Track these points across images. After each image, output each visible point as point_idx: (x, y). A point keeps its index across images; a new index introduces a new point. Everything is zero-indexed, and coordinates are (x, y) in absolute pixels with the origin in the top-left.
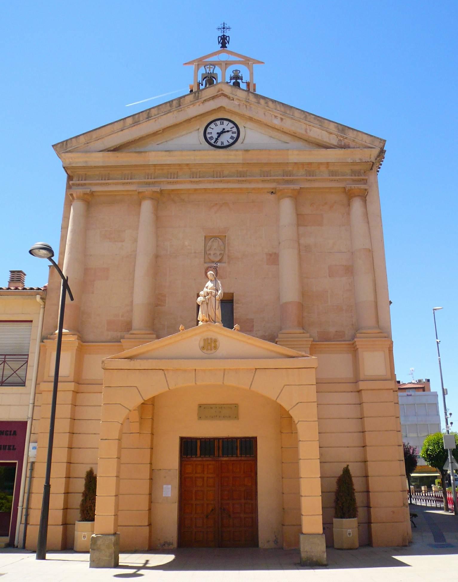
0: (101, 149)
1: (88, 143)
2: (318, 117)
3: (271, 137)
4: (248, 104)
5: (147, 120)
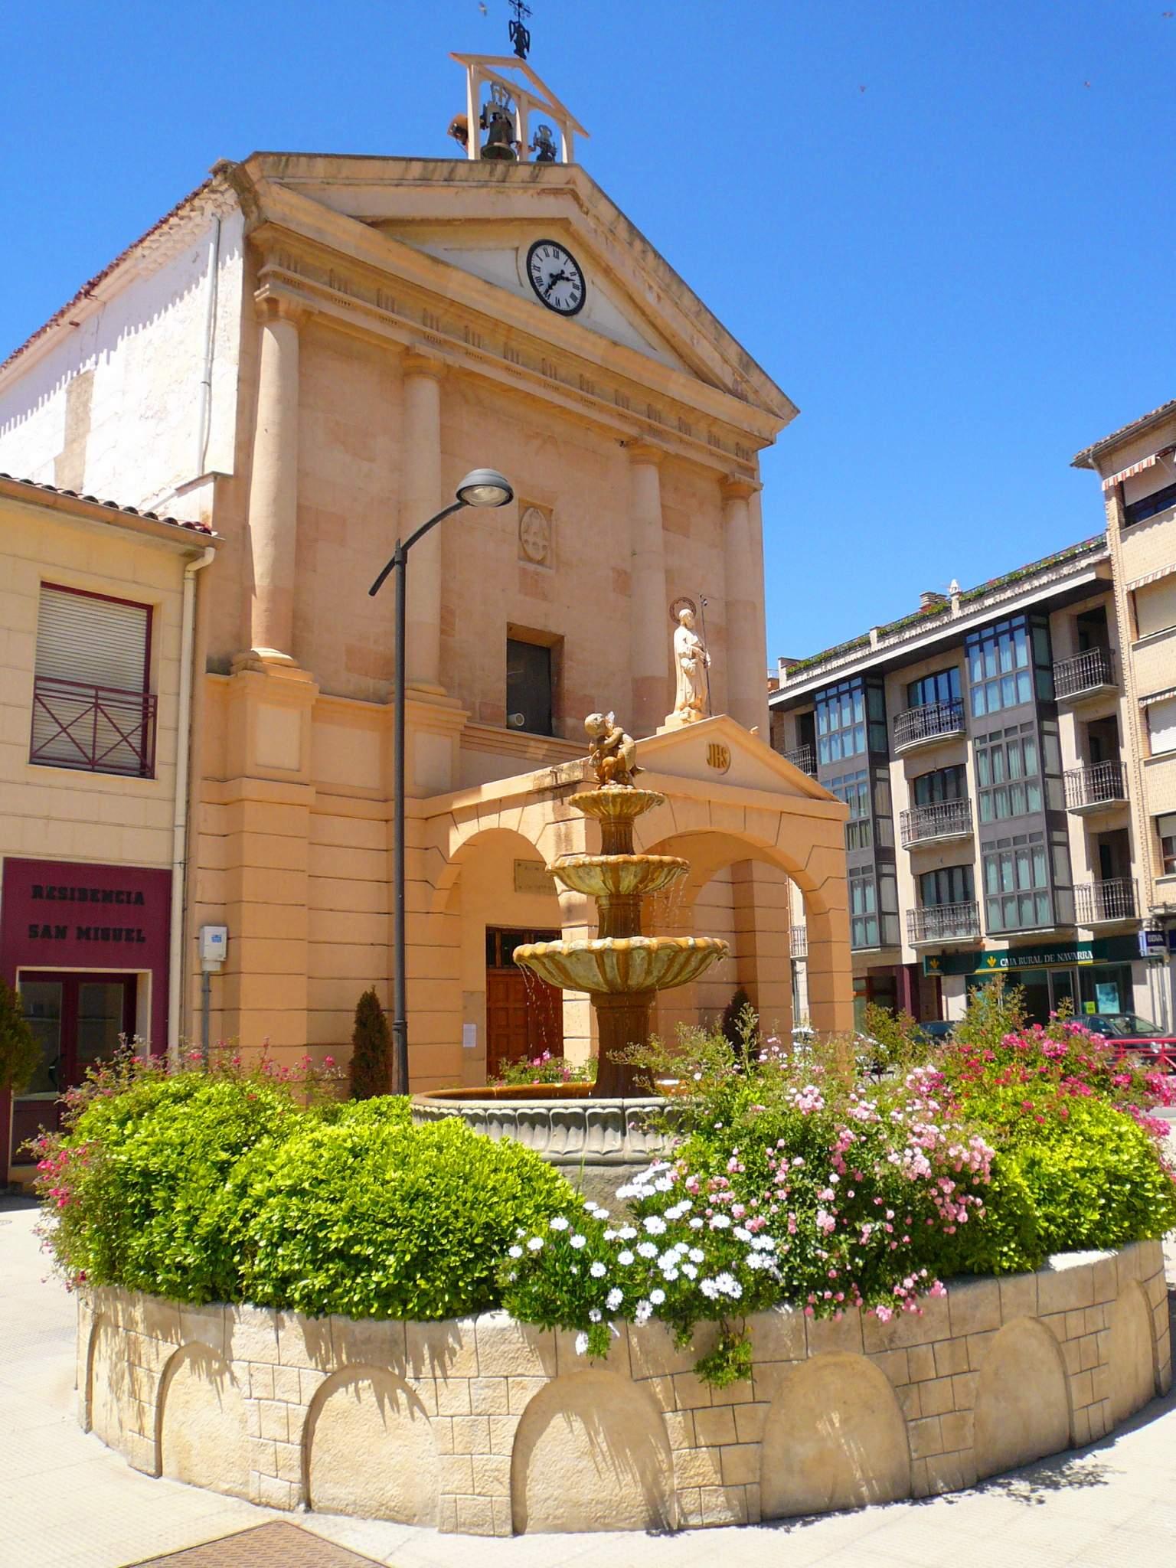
0: (354, 214)
1: (328, 184)
2: (719, 322)
3: (631, 325)
5: (446, 183)
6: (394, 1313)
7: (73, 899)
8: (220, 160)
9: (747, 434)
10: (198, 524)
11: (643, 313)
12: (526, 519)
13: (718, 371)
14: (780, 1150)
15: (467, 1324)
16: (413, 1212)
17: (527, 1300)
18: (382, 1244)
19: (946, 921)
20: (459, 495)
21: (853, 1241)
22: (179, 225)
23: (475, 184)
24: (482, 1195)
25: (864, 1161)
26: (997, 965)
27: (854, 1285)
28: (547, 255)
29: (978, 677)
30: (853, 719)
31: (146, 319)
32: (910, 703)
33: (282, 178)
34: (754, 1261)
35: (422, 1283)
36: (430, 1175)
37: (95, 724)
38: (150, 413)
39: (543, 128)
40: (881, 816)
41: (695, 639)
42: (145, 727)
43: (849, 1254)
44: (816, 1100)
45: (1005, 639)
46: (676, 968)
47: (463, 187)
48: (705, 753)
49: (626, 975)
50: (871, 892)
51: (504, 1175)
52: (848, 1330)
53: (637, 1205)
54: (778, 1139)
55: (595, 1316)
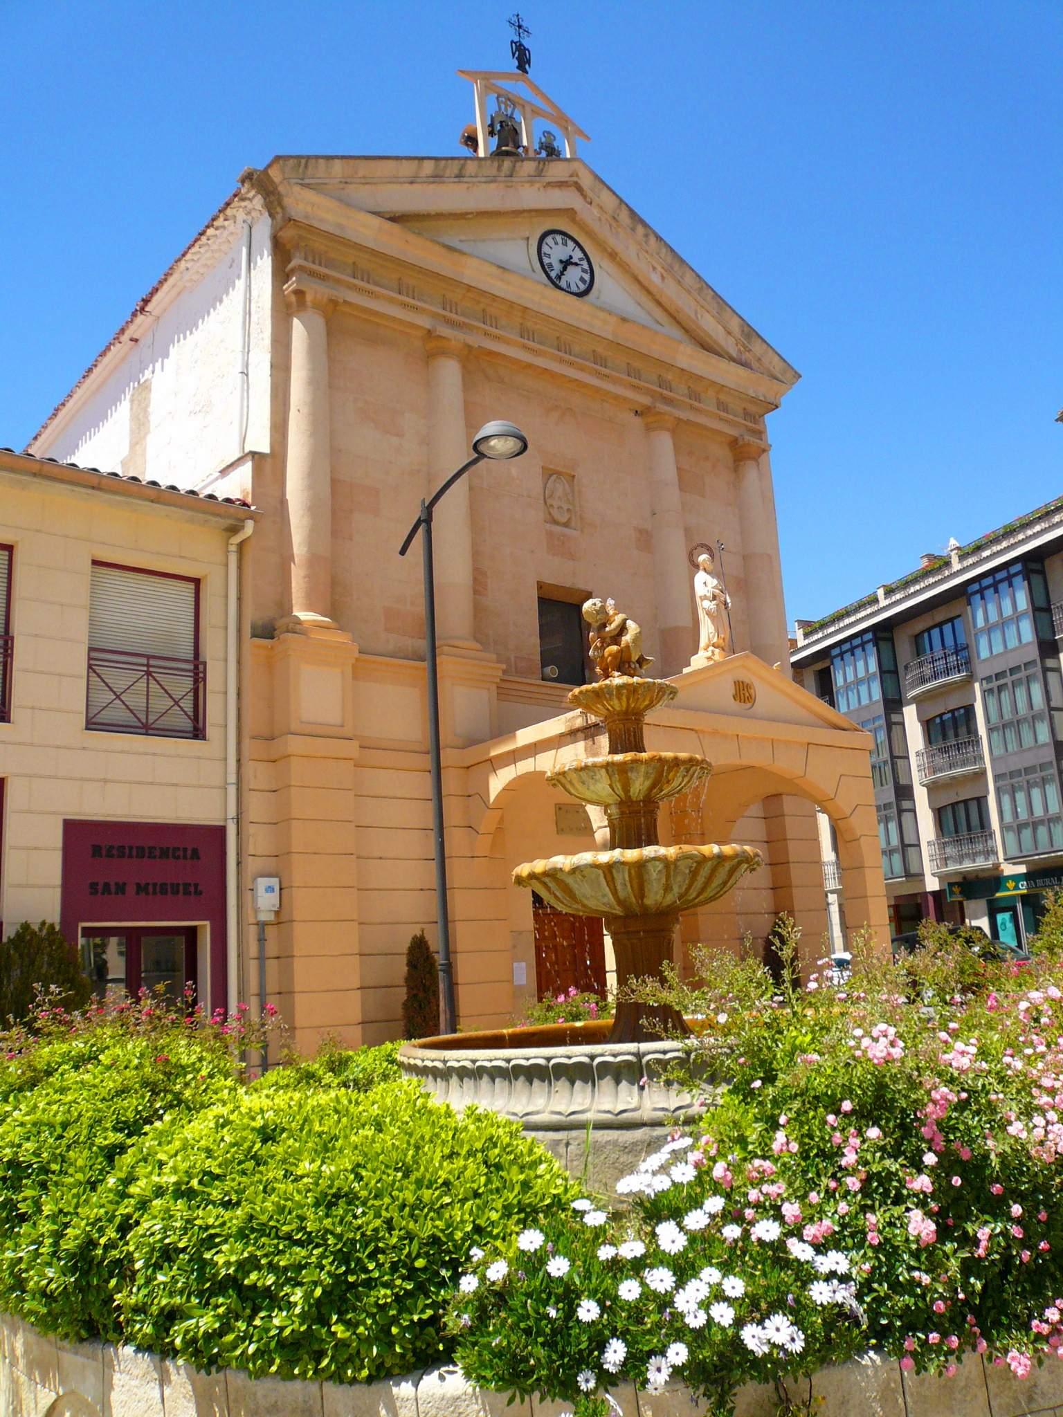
1: (346, 183)
2: (720, 297)
4: (614, 224)
5: (456, 180)
6: (304, 1373)
7: (130, 856)
8: (245, 168)
9: (754, 400)
10: (239, 500)
11: (649, 292)
12: (550, 484)
13: (723, 343)
14: (846, 1115)
15: (404, 1390)
16: (327, 1222)
17: (487, 1356)
18: (286, 1269)
19: (965, 851)
20: (475, 447)
21: (965, 1254)
22: (216, 236)
23: (484, 179)
24: (427, 1194)
25: (969, 1129)
26: (1016, 888)
27: (969, 1317)
28: (556, 244)
29: (980, 622)
30: (867, 670)
31: (192, 325)
32: (919, 652)
33: (302, 179)
34: (821, 1293)
35: (339, 1330)
36: (358, 1165)
37: (148, 691)
38: (198, 408)
39: (547, 133)
40: (898, 757)
41: (715, 582)
42: (196, 691)
43: (962, 1273)
44: (893, 1044)
45: (1003, 586)
46: (700, 881)
47: (474, 183)
48: (731, 690)
49: (641, 893)
50: (893, 826)
51: (462, 1163)
52: (966, 1386)
53: (648, 1205)
54: (842, 1100)
55: (586, 1381)
